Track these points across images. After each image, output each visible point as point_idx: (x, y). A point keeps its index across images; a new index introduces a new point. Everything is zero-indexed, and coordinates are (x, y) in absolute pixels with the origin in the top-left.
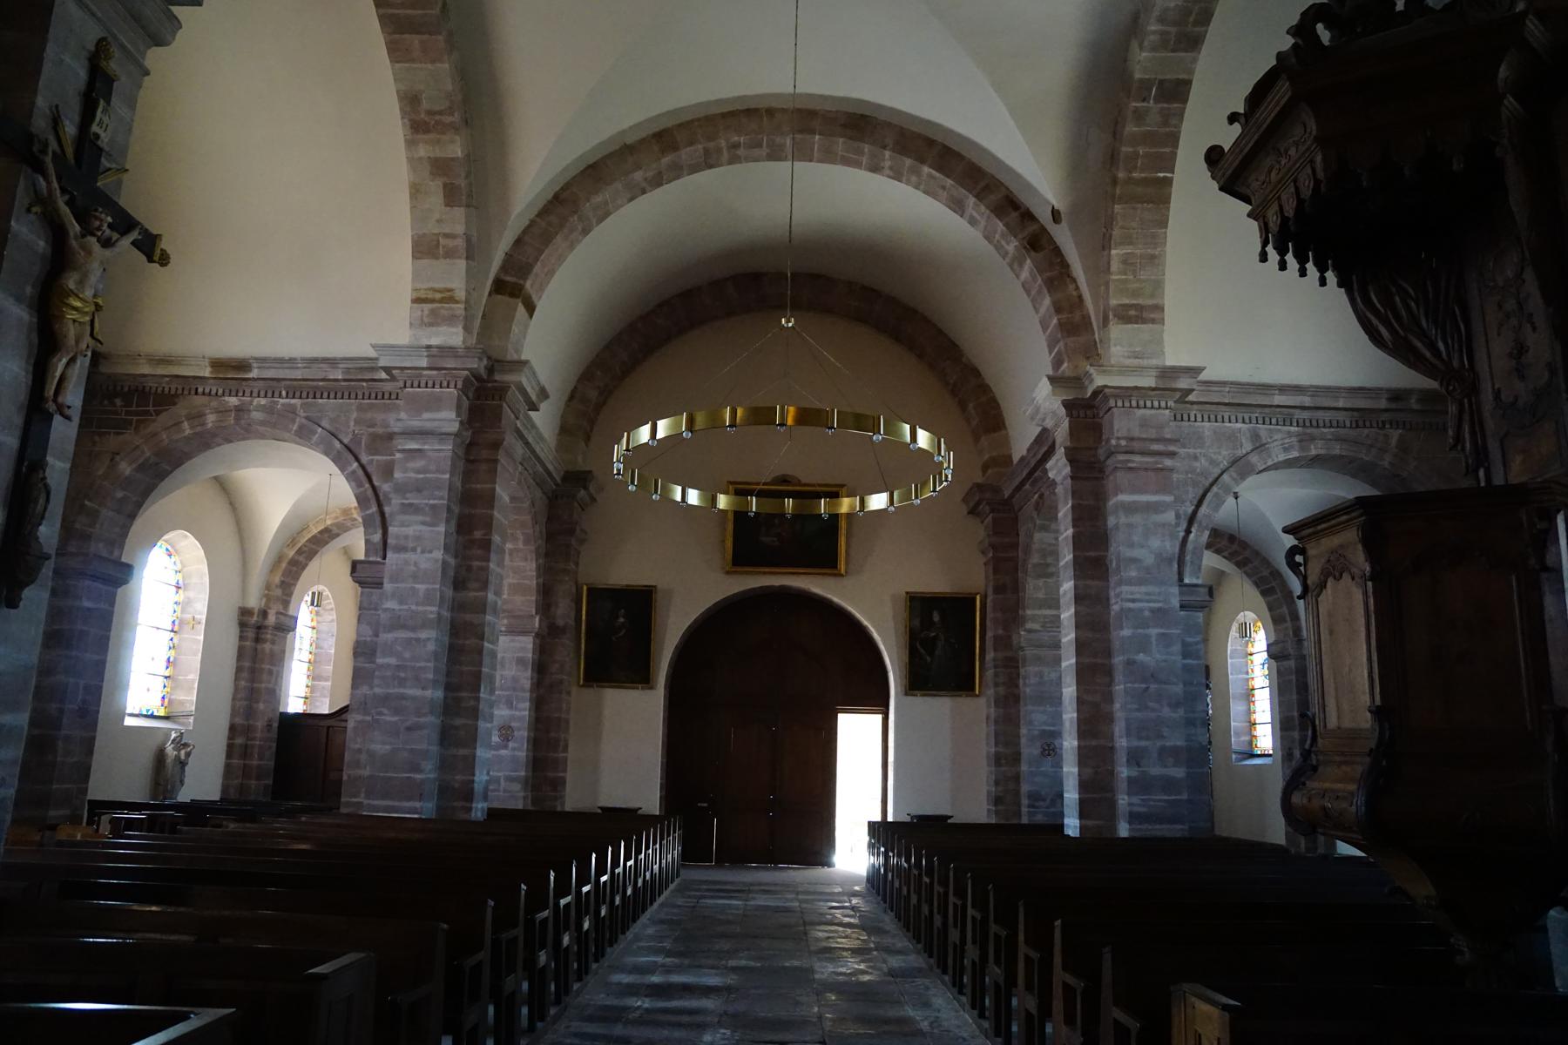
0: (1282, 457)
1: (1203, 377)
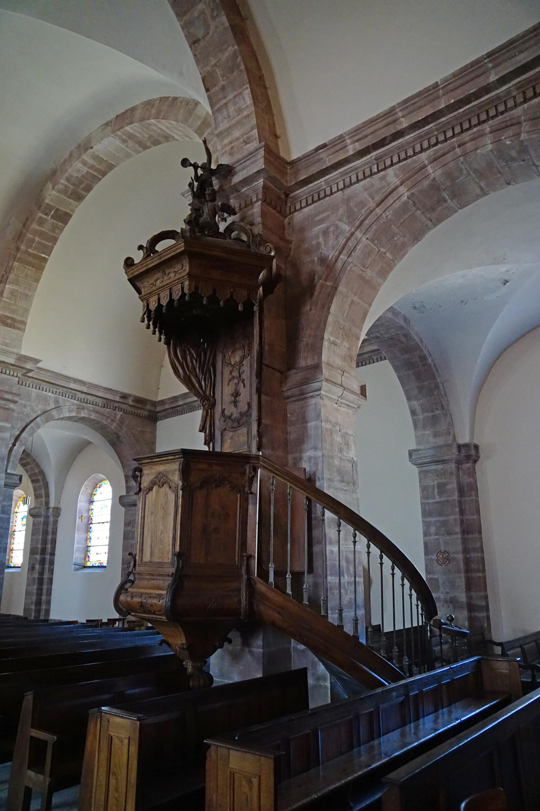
0: (67, 415)
1: (40, 365)
